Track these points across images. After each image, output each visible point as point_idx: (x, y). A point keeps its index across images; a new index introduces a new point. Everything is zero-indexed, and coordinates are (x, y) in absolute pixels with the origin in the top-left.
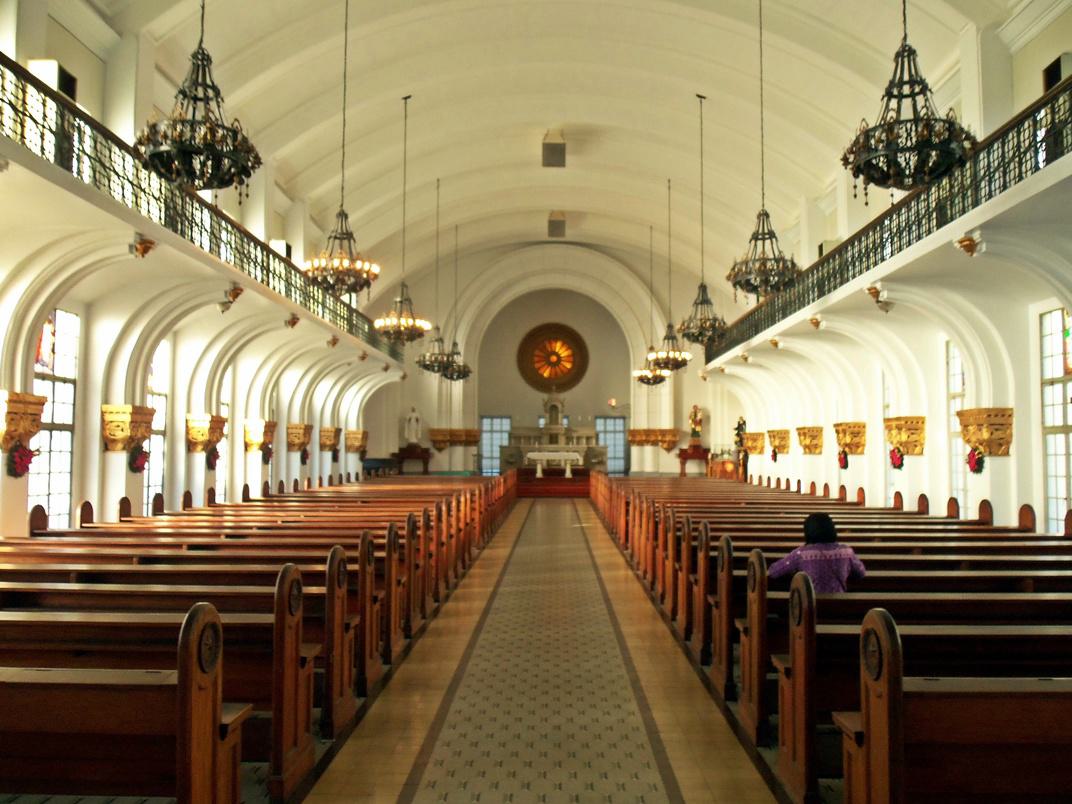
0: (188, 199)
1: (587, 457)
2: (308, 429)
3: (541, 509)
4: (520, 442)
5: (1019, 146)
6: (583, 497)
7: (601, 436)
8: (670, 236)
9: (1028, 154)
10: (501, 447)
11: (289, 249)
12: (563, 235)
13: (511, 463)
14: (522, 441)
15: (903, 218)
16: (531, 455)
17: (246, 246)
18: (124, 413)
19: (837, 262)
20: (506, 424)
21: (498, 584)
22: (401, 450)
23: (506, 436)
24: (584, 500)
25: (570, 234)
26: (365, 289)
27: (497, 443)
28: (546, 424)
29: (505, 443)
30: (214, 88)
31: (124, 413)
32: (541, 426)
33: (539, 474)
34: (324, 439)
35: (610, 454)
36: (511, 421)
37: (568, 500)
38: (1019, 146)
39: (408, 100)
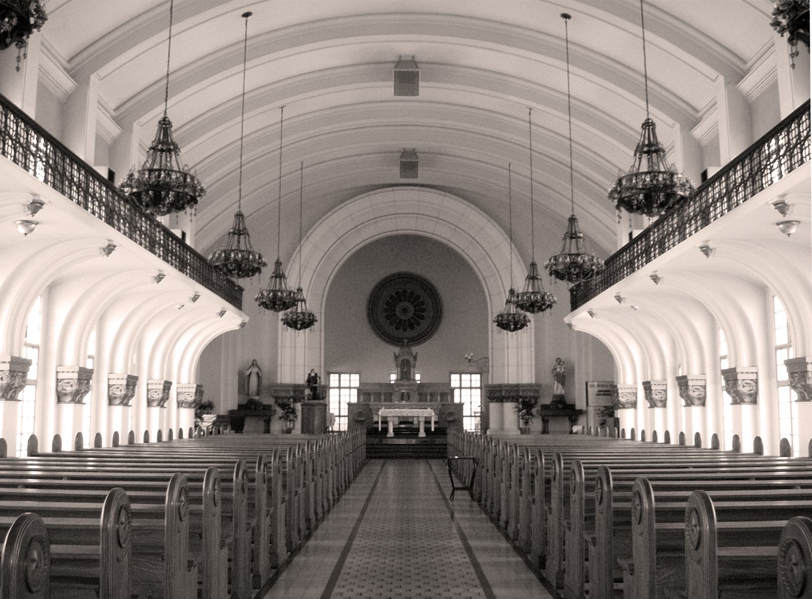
0: (91, 179)
2: (167, 386)
5: (799, 135)
7: (457, 392)
9: (795, 150)
10: (350, 404)
12: (416, 176)
13: (361, 422)
15: (739, 174)
18: (122, 379)
22: (240, 406)
23: (354, 392)
25: (424, 174)
26: (257, 274)
27: (345, 400)
28: (397, 380)
29: (354, 400)
30: (173, 143)
32: (392, 382)
35: (466, 412)
38: (799, 135)
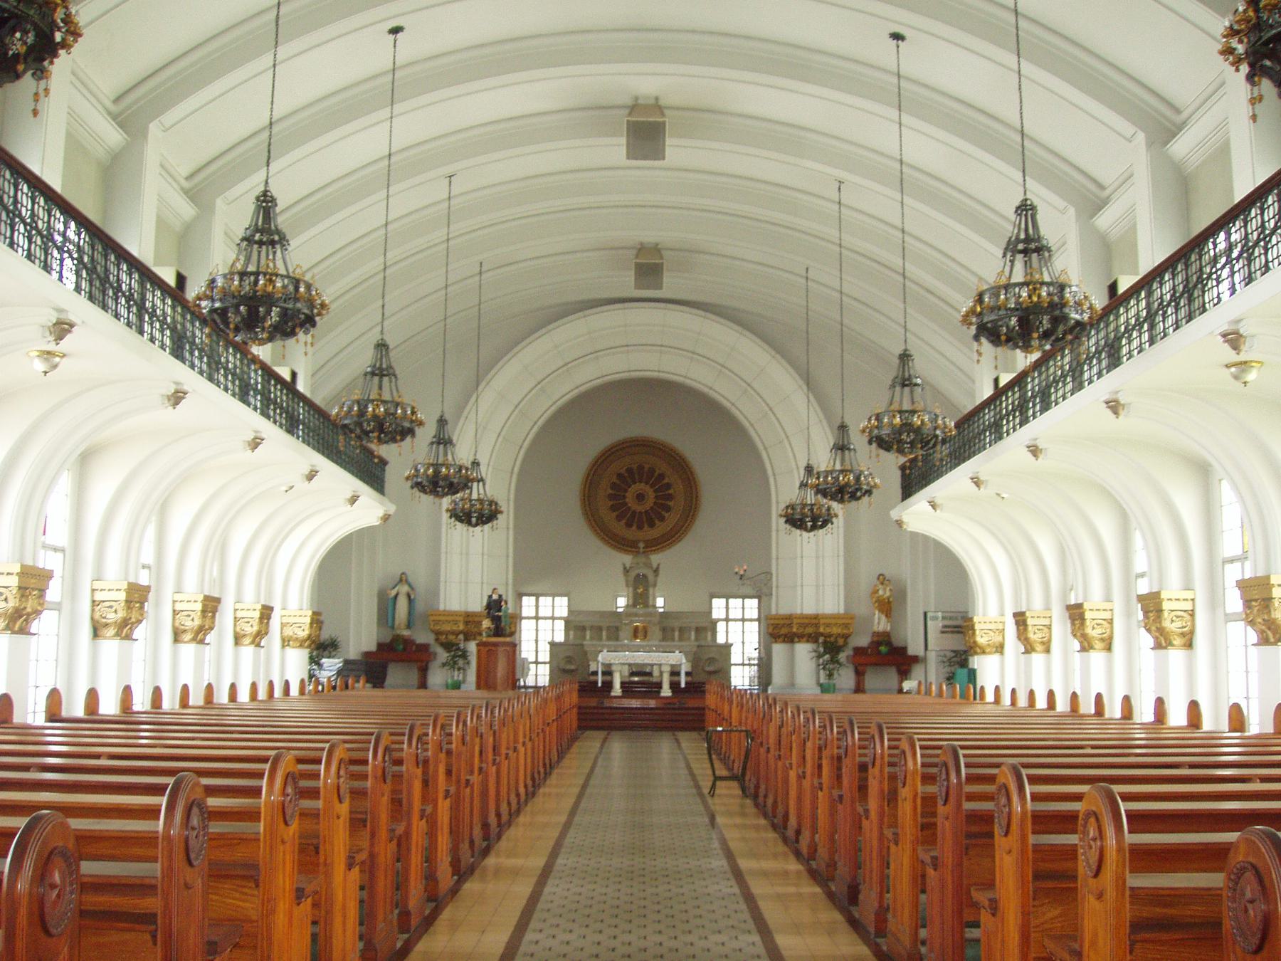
1: (695, 660)
3: (618, 747)
4: (584, 638)
6: (694, 729)
8: (902, 203)
11: (294, 375)
14: (588, 634)
16: (604, 657)
17: (113, 269)
18: (195, 601)
19: (1067, 359)
20: (561, 606)
21: (554, 854)
22: (380, 646)
23: (560, 625)
24: (694, 735)
25: (671, 284)
27: (545, 639)
28: (627, 606)
29: (560, 637)
31: (195, 601)
32: (620, 610)
33: (600, 685)
34: (241, 625)
35: (735, 657)
36: (569, 600)
37: (669, 734)
39: (400, 35)
